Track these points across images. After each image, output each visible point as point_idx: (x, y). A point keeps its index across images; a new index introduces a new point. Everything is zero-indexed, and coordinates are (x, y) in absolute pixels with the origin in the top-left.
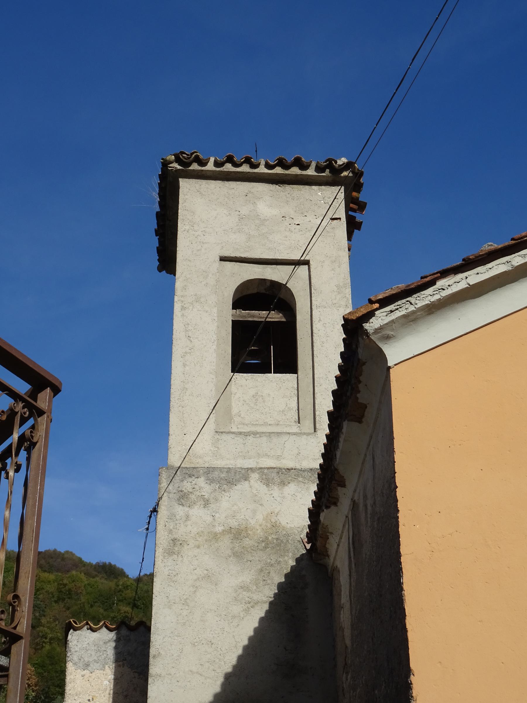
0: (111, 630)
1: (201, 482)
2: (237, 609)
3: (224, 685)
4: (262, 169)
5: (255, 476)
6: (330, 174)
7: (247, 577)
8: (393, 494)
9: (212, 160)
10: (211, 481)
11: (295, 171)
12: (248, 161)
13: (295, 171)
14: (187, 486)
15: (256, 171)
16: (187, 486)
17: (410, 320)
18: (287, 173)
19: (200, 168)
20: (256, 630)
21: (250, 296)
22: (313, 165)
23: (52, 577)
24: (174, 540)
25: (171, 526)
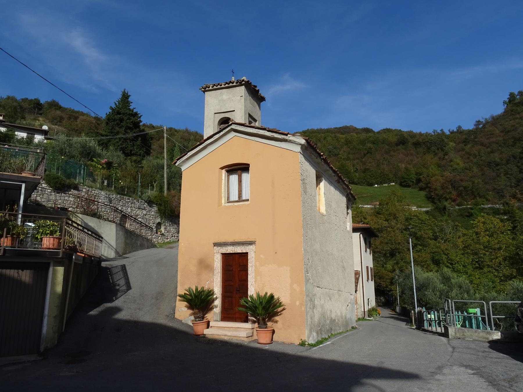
4: (223, 86)
6: (240, 83)
8: (176, 198)
11: (231, 84)
13: (231, 84)
18: (229, 85)
23: (344, 136)
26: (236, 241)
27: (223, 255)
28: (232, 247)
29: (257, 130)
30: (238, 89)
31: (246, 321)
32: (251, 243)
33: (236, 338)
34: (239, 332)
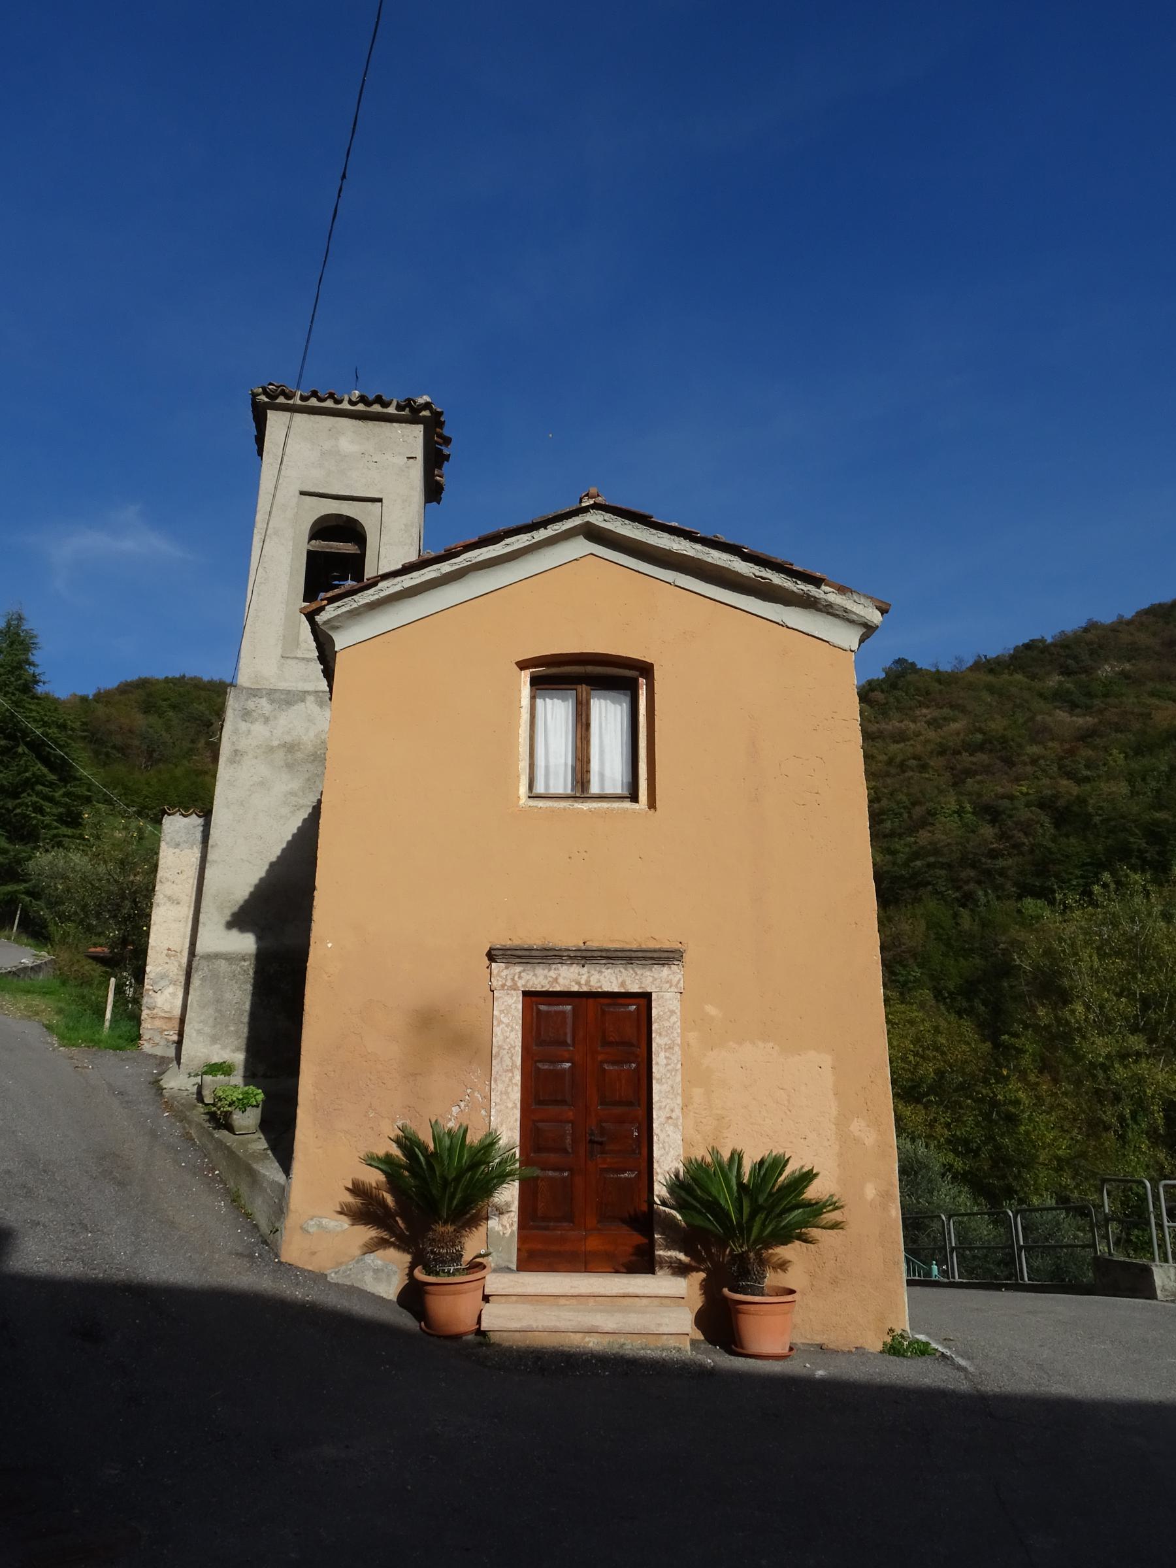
0: (199, 817)
1: (264, 701)
2: (285, 811)
3: (268, 872)
4: (345, 405)
5: (310, 698)
6: (410, 413)
7: (295, 785)
9: (298, 394)
10: (272, 701)
11: (377, 408)
12: (331, 396)
13: (377, 408)
14: (251, 705)
15: (339, 406)
16: (251, 705)
17: (355, 614)
18: (370, 410)
19: (286, 401)
20: (299, 829)
21: (327, 528)
22: (394, 403)
24: (236, 751)
25: (234, 739)
26: (594, 944)
27: (529, 995)
28: (575, 969)
29: (698, 547)
30: (398, 429)
31: (644, 1264)
32: (666, 957)
33: (638, 1342)
34: (649, 1311)
